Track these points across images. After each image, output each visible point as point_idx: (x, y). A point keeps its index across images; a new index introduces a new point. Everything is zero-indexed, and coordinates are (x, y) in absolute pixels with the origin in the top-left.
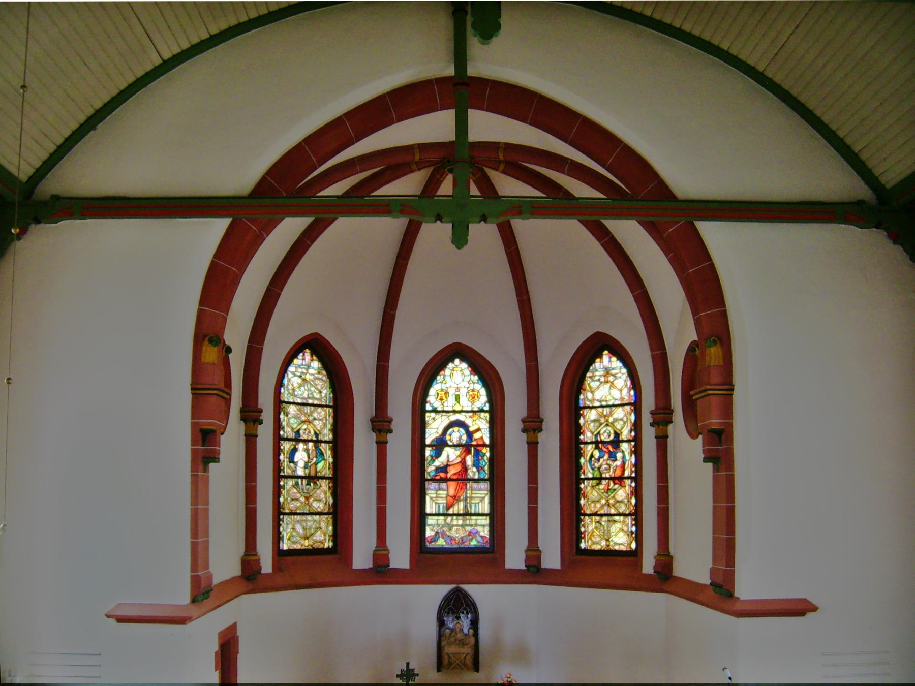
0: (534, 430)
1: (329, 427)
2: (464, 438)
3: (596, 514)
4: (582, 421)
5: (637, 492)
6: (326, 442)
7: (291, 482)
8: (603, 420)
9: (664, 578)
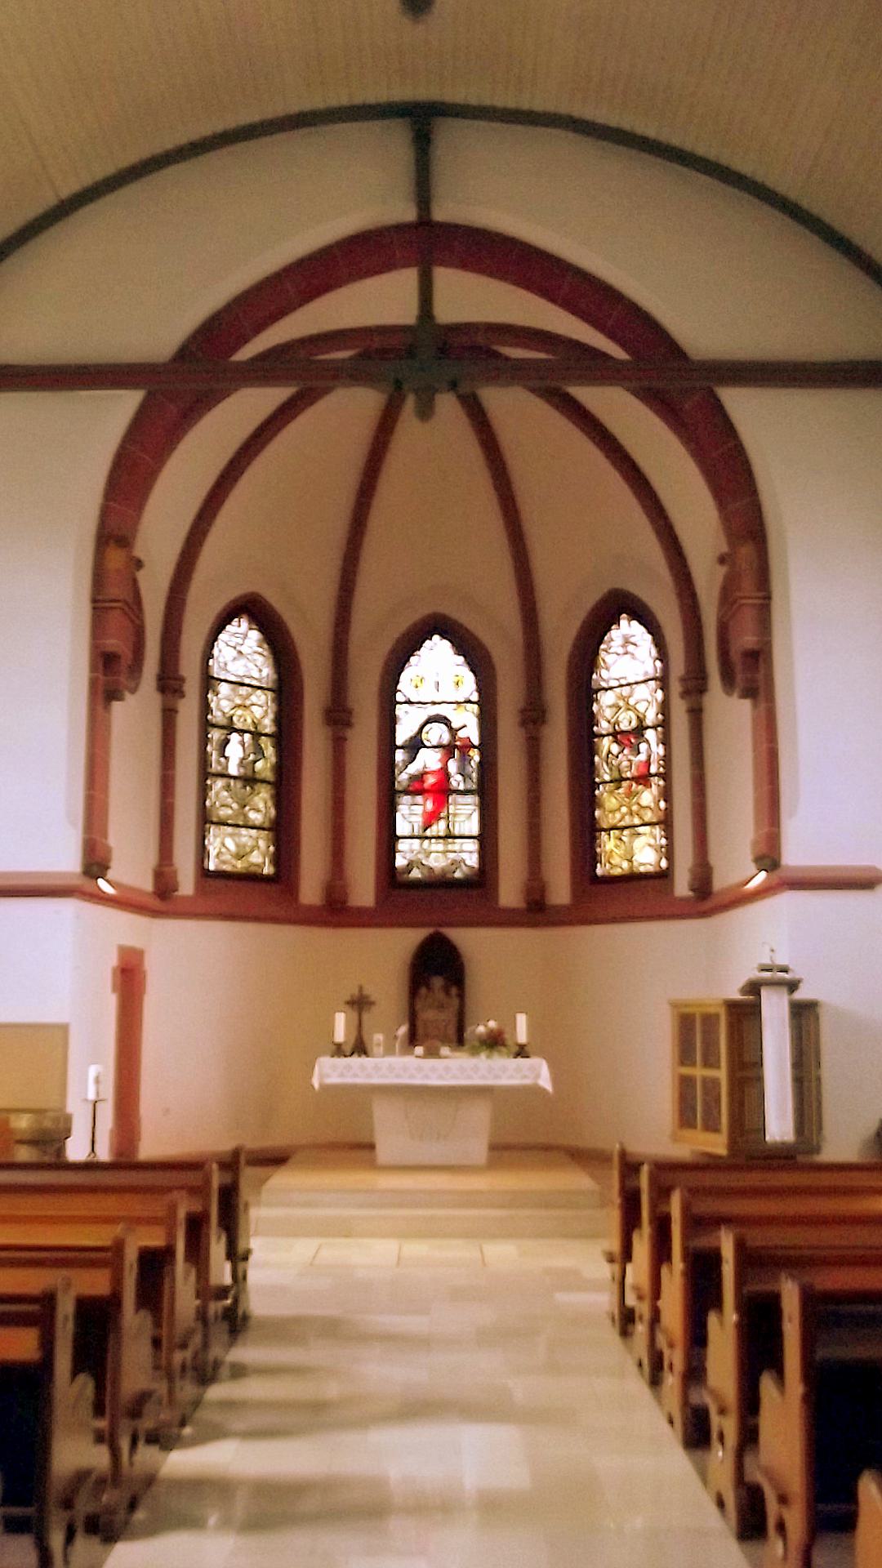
0: (535, 722)
1: (271, 716)
3: (614, 828)
4: (595, 708)
5: (666, 794)
6: (266, 735)
7: (220, 783)
8: (621, 703)
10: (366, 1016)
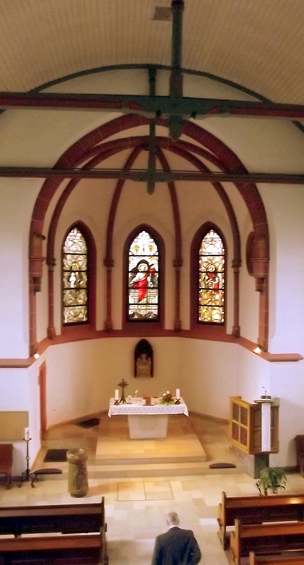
1: (85, 264)
2: (147, 268)
3: (206, 305)
4: (200, 262)
5: (225, 296)
6: (83, 271)
7: (68, 292)
9: (236, 336)
10: (125, 389)
